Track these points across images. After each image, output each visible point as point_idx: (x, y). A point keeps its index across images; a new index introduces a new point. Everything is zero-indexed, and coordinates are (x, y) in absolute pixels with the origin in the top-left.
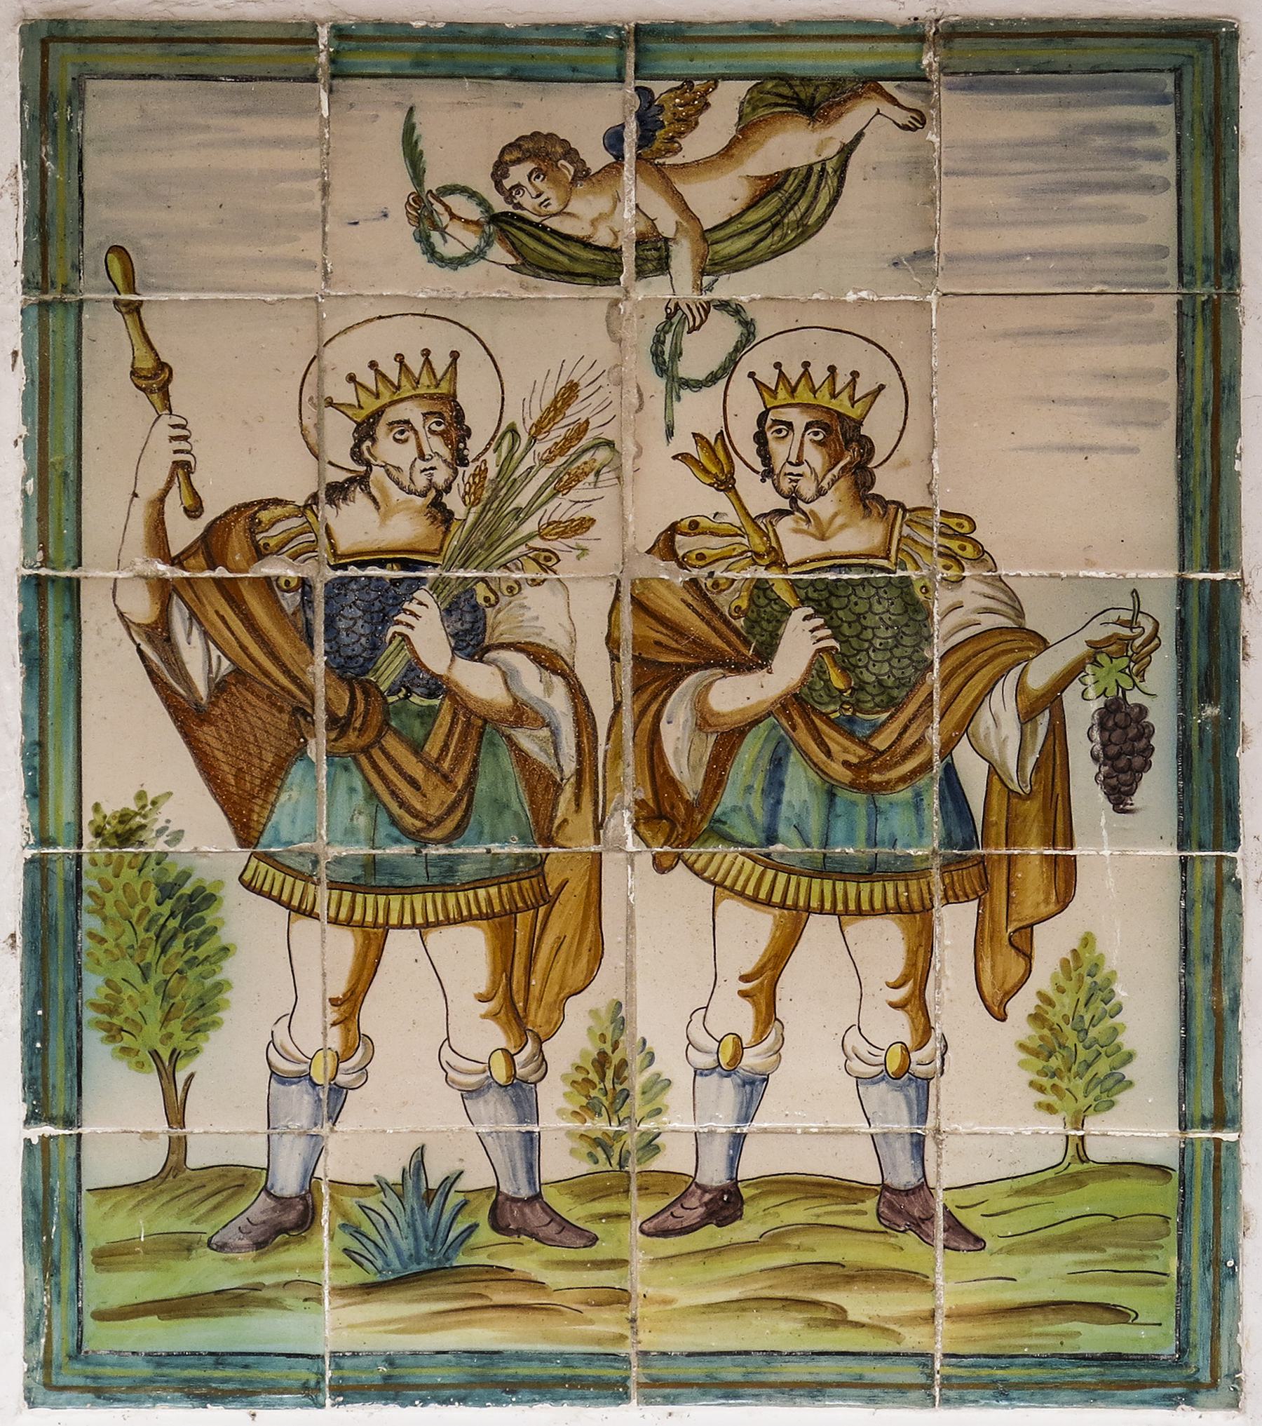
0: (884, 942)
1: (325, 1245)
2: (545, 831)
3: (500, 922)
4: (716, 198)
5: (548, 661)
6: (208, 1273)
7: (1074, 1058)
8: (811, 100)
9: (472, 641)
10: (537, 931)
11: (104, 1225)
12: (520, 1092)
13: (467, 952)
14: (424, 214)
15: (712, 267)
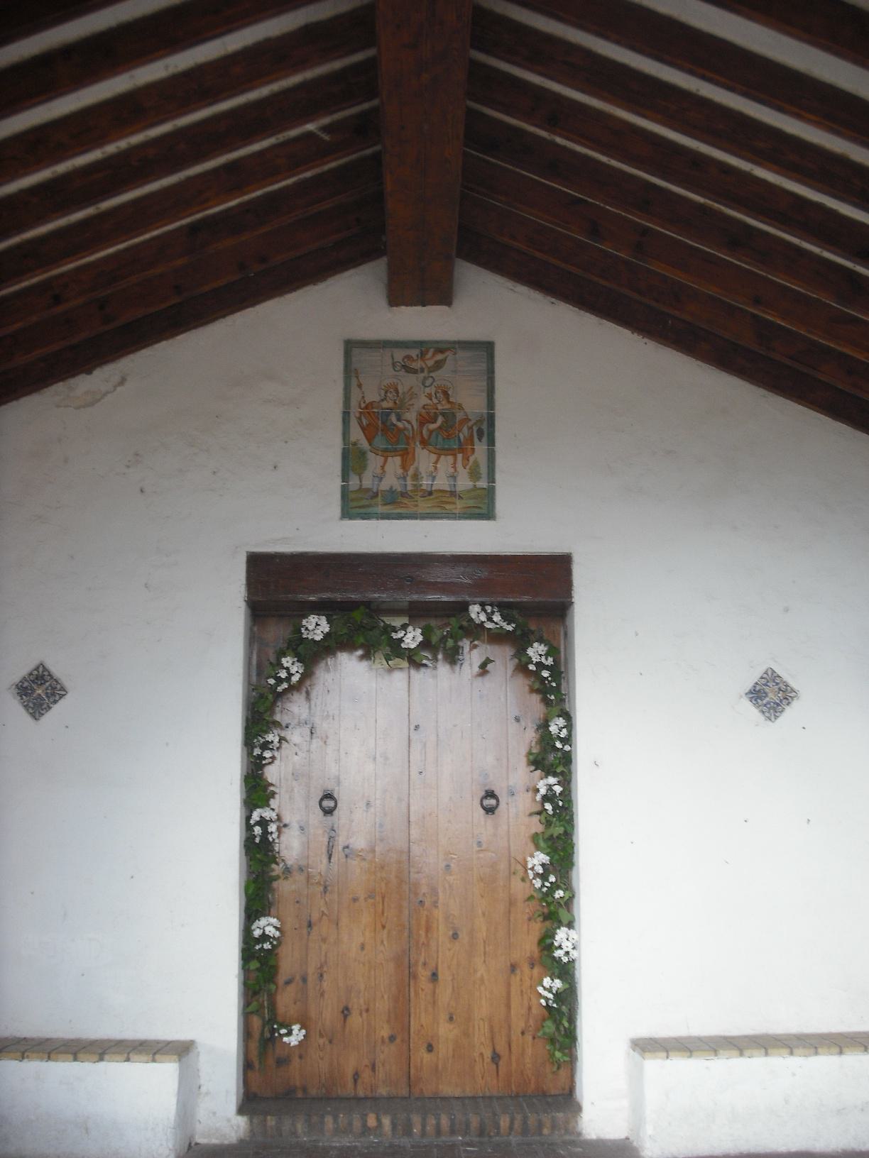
0: (450, 459)
1: (379, 498)
2: (408, 444)
3: (402, 456)
4: (430, 363)
5: (409, 422)
6: (364, 502)
7: (474, 475)
8: (441, 351)
9: (399, 420)
10: (407, 457)
11: (352, 496)
12: (404, 478)
13: (398, 460)
14: (394, 365)
15: (430, 372)
